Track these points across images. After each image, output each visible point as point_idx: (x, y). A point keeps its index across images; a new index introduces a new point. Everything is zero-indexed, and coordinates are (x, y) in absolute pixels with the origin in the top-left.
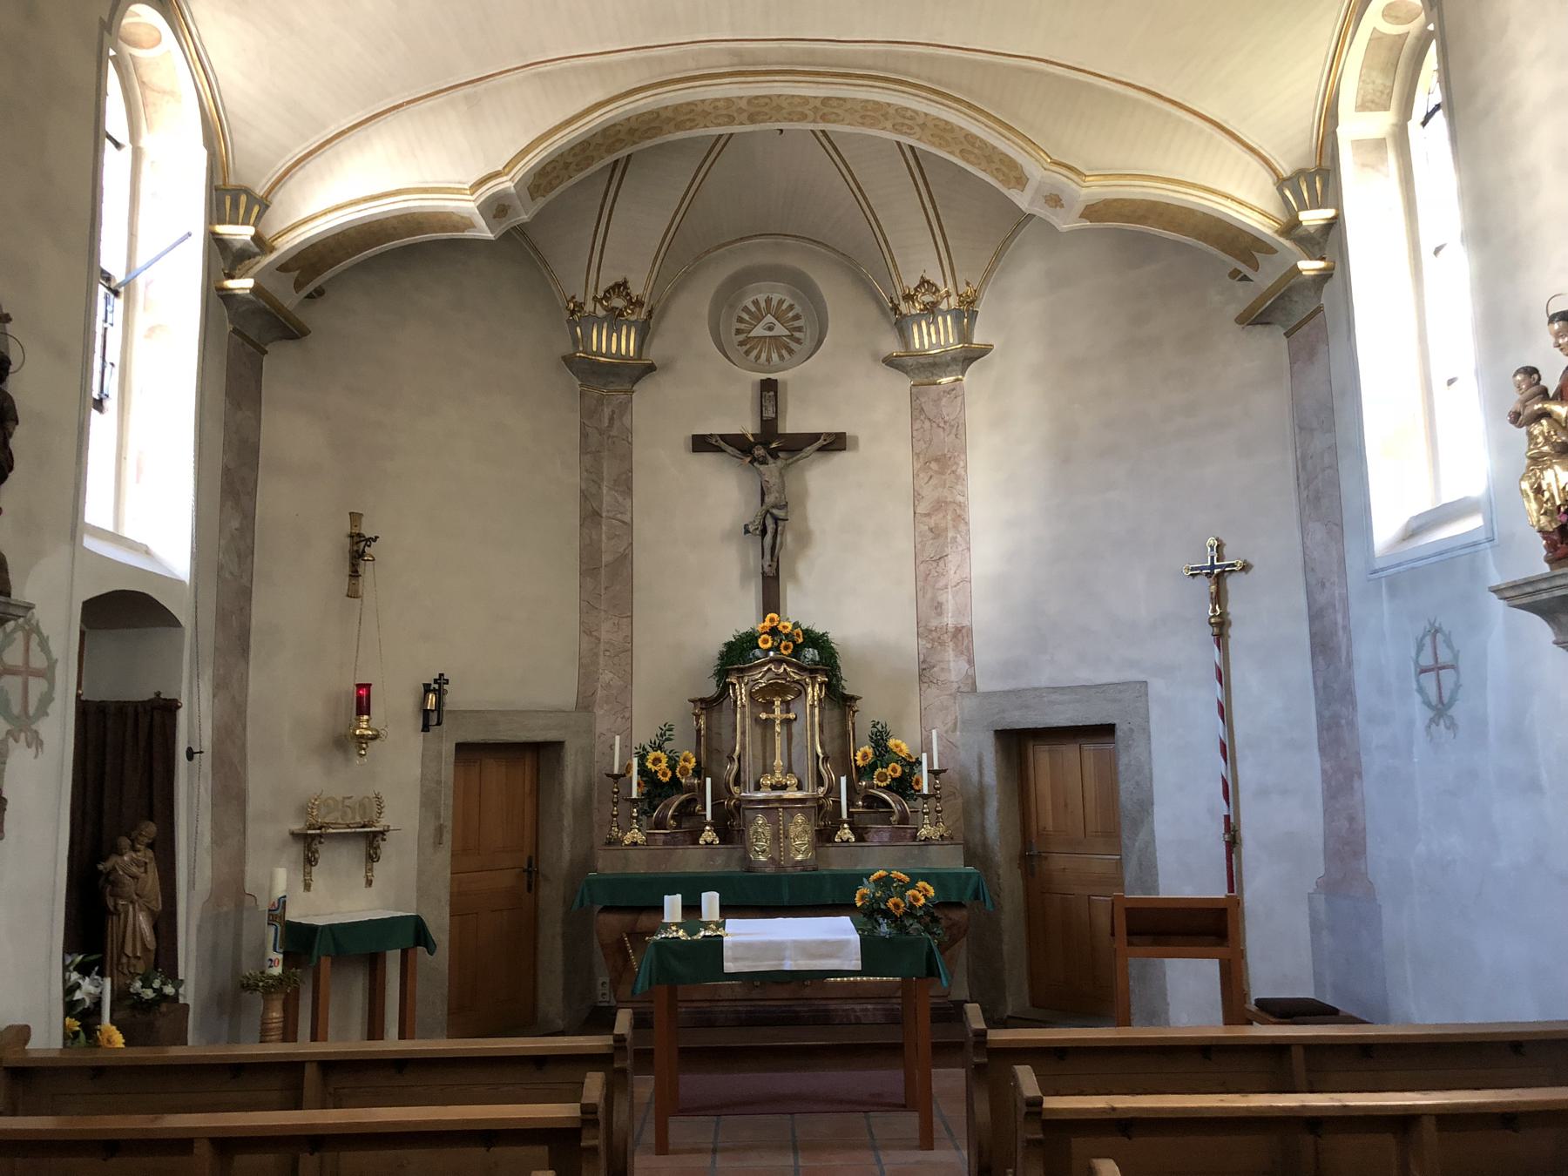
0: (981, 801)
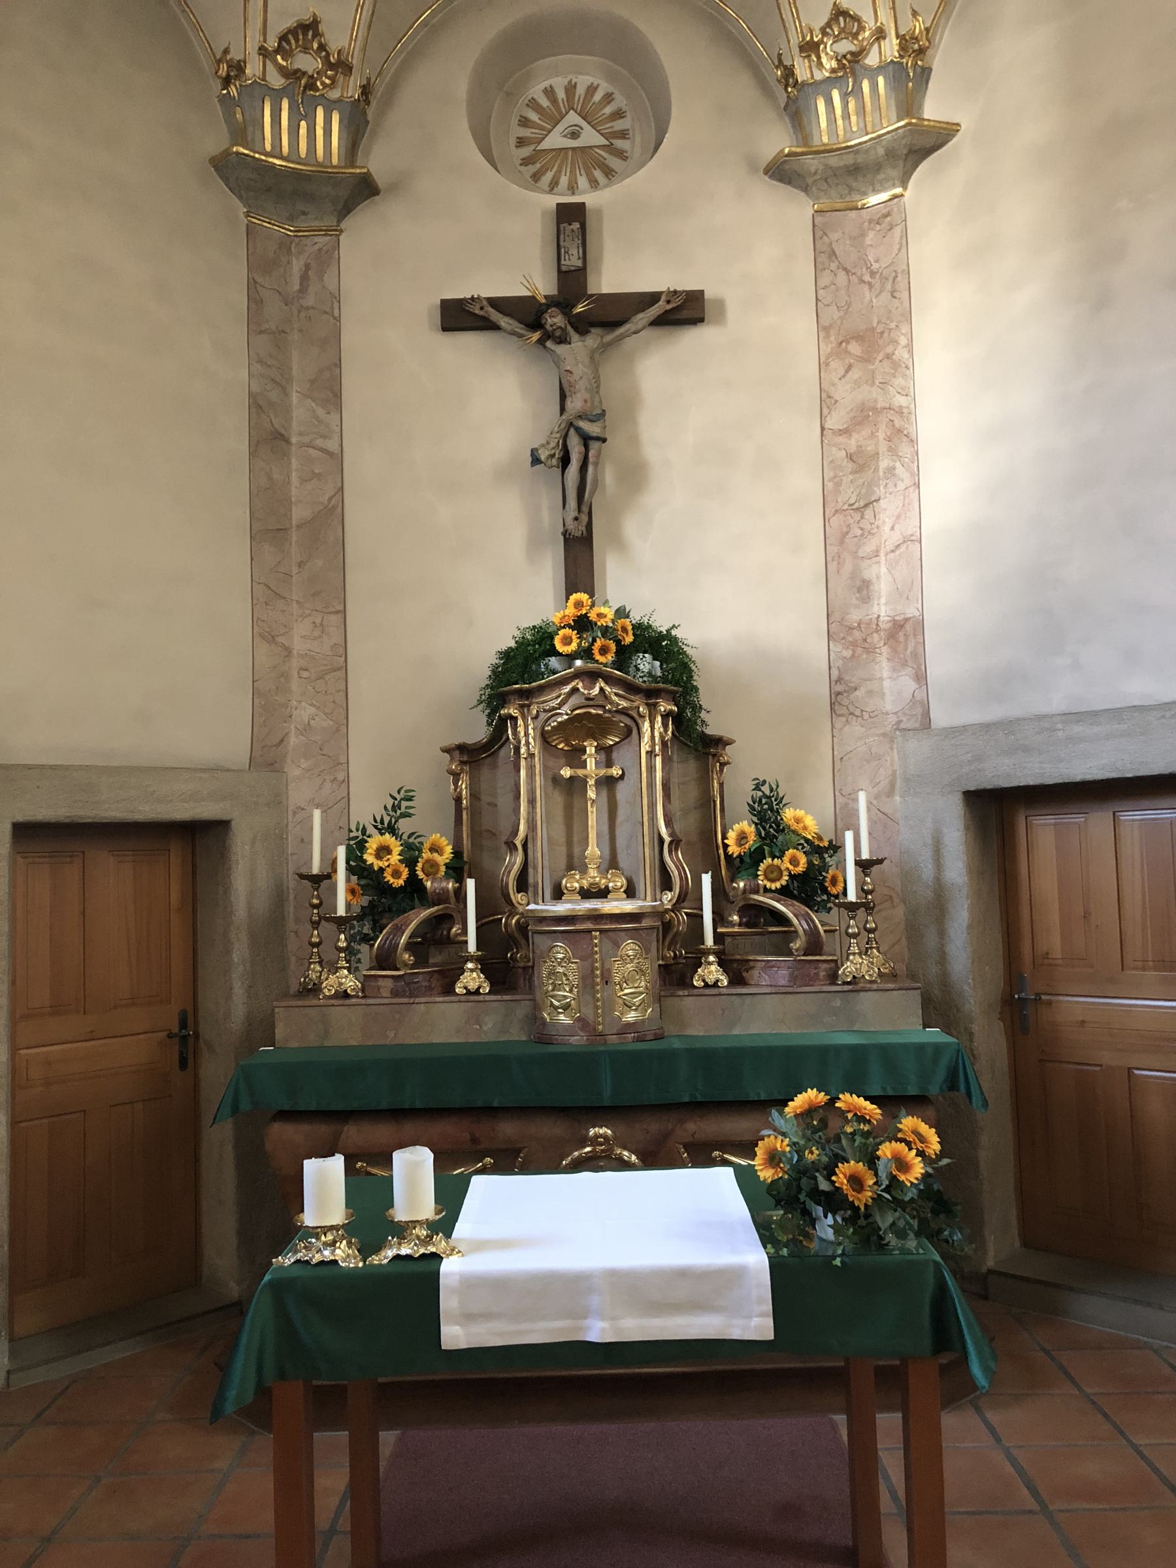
0: (939, 905)
